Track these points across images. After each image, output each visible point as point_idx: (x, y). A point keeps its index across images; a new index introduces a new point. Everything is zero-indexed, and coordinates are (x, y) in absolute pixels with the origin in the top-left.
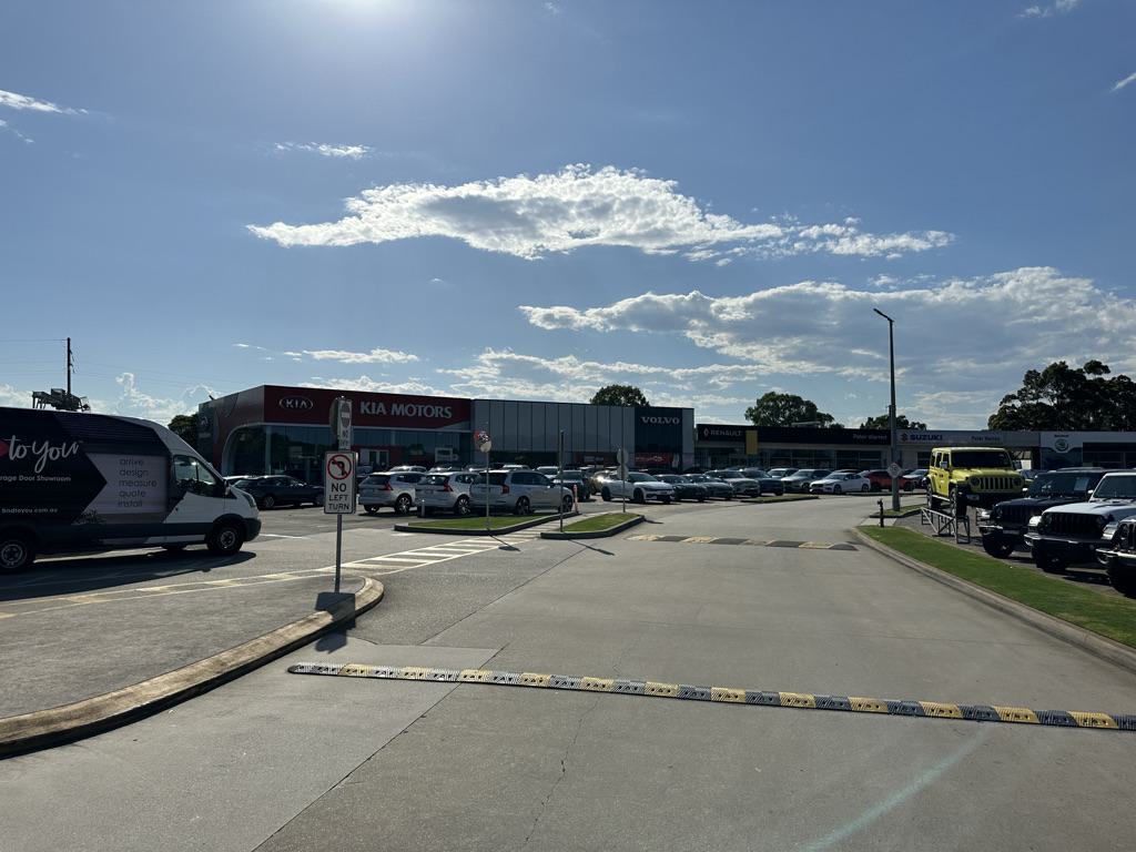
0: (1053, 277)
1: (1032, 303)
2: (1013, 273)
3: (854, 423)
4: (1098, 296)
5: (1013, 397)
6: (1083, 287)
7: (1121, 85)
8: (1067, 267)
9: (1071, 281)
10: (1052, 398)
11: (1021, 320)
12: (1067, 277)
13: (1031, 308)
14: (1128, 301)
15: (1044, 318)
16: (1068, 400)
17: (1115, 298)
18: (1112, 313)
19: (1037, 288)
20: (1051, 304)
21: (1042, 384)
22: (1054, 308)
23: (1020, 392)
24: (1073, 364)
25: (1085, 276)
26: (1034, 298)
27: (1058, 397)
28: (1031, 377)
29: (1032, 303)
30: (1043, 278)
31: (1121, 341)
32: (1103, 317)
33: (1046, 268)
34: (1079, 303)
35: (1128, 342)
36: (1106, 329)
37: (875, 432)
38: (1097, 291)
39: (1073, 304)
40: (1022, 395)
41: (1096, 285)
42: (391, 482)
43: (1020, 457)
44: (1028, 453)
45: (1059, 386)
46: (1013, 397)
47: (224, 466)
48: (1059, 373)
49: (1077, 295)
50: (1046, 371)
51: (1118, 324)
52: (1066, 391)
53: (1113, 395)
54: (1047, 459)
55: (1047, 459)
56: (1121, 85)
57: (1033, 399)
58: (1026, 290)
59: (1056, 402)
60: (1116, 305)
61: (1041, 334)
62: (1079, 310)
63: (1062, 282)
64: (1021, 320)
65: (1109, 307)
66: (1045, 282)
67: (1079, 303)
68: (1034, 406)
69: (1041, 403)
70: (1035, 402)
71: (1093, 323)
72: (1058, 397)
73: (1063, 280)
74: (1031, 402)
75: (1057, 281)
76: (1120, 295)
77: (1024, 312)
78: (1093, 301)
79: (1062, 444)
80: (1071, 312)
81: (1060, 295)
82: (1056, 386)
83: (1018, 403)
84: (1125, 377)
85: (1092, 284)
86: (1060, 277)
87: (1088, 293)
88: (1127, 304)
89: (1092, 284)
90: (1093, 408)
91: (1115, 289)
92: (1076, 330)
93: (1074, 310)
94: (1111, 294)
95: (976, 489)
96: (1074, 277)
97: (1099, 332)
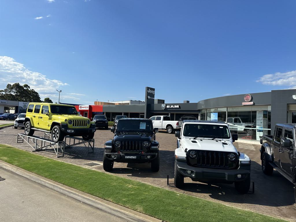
0: (14, 61)
1: (7, 67)
2: (2, 57)
3: (21, 82)
4: (24, 69)
5: (3, 91)
6: (21, 66)
7: (37, 18)
8: (17, 59)
9: (18, 63)
10: (15, 92)
11: (3, 71)
12: (17, 62)
13: (6, 68)
14: (31, 72)
15: (10, 72)
16: (19, 94)
17: (28, 70)
18: (27, 74)
19: (8, 63)
20: (12, 68)
21: (12, 88)
22: (13, 69)
23: (5, 90)
24: (22, 84)
25: (22, 63)
26: (7, 66)
27: (16, 93)
28: (9, 86)
29: (8, 67)
30: (11, 61)
31: (28, 81)
32: (25, 75)
33: (12, 58)
34: (19, 69)
35: (30, 82)
36: (25, 78)
37: (27, 92)
38: (24, 68)
39: (18, 70)
40: (6, 90)
41: (24, 66)
42: (269, 115)
43: (11, 109)
44: (14, 108)
45: (17, 90)
46: (3, 91)
47: (129, 117)
48: (17, 86)
49: (19, 67)
50: (14, 85)
51: (28, 77)
52: (18, 91)
53: (30, 94)
54: (20, 110)
55: (20, 110)
56: (37, 18)
57: (8, 92)
58: (5, 62)
59: (15, 94)
60: (28, 72)
61: (8, 76)
62: (19, 72)
63: (16, 63)
64: (3, 71)
65: (27, 72)
66: (11, 62)
67: (19, 69)
68: (9, 94)
69: (11, 94)
70: (9, 93)
71: (22, 76)
72: (16, 93)
73: (16, 62)
74: (8, 93)
75: (14, 62)
76: (29, 70)
77: (4, 68)
78: (23, 70)
79: (25, 106)
80: (17, 72)
81: (15, 66)
82: (16, 90)
83: (4, 93)
84: (33, 90)
85: (23, 65)
86: (15, 62)
87: (22, 68)
88: (31, 73)
89: (23, 65)
90: (25, 97)
91: (29, 68)
92: (18, 76)
93: (18, 71)
94: (28, 69)
95: (70, 126)
96: (19, 62)
97: (23, 78)
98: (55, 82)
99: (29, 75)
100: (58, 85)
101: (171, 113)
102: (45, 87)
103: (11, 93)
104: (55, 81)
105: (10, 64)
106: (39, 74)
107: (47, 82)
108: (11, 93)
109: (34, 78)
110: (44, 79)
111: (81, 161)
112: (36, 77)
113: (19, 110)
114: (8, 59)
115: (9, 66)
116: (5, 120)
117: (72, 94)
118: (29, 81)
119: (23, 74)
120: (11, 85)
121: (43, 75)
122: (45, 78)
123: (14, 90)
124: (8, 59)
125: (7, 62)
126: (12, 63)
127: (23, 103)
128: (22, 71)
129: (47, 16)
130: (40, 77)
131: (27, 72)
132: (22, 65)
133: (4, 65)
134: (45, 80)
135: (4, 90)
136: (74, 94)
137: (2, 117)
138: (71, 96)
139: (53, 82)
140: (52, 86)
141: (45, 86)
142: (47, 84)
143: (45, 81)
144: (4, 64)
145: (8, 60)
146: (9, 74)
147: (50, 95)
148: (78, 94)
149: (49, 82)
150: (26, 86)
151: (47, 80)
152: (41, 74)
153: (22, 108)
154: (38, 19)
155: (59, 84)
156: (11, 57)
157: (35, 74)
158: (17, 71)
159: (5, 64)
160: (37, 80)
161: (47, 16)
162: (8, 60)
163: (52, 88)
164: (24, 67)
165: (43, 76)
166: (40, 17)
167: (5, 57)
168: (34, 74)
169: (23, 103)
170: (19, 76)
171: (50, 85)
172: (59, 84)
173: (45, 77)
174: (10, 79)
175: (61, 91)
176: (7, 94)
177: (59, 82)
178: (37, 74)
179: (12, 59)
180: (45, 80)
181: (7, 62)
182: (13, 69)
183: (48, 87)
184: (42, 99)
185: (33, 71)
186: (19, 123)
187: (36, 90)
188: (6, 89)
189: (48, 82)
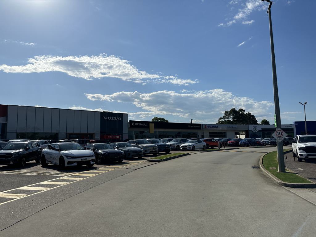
0: (224, 91)
5: (222, 118)
6: (230, 94)
7: (240, 45)
8: (226, 89)
9: (227, 92)
11: (216, 102)
12: (226, 91)
13: (218, 99)
15: (221, 101)
18: (236, 100)
19: (219, 94)
21: (229, 114)
22: (223, 99)
23: (223, 117)
24: (237, 110)
27: (234, 118)
29: (219, 98)
31: (238, 107)
32: (234, 102)
34: (229, 98)
38: (233, 95)
39: (228, 98)
43: (241, 134)
48: (233, 111)
49: (229, 96)
51: (237, 103)
56: (240, 45)
58: (217, 94)
61: (220, 106)
62: (229, 100)
63: (225, 92)
65: (235, 99)
67: (229, 98)
72: (234, 118)
73: (225, 92)
76: (237, 96)
78: (232, 97)
80: (227, 100)
81: (225, 96)
82: (233, 115)
83: (223, 120)
84: (250, 113)
87: (231, 96)
88: (239, 98)
92: (228, 105)
93: (228, 99)
96: (228, 91)
98: (264, 103)
99: (238, 101)
100: (267, 106)
101: (296, 135)
102: (254, 110)
103: (229, 119)
104: (264, 102)
105: (221, 95)
106: (247, 98)
107: (256, 105)
108: (229, 119)
109: (242, 103)
110: (252, 103)
111: (299, 190)
112: (244, 102)
113: (249, 135)
114: (219, 91)
115: (220, 96)
116: (248, 146)
117: (285, 113)
118: (238, 107)
119: (232, 101)
120: (228, 112)
121: (251, 99)
122: (253, 101)
123: (231, 116)
124: (219, 91)
125: (218, 93)
126: (222, 93)
127: (253, 126)
128: (231, 99)
129: (249, 39)
130: (248, 101)
131: (235, 99)
132: (231, 93)
133: (216, 97)
134: (254, 103)
135: (223, 117)
136: (287, 113)
137: (243, 143)
138: (284, 116)
139: (262, 104)
140: (261, 109)
141: (254, 109)
142: (256, 107)
143: (254, 104)
144: (216, 95)
145: (219, 92)
146: (221, 104)
147: (260, 118)
148: (292, 112)
149: (258, 104)
150: (241, 110)
151: (255, 103)
152: (248, 98)
153: (253, 131)
154: (241, 45)
155: (269, 105)
156: (221, 89)
157: (243, 100)
158: (227, 99)
159: (217, 96)
160: (245, 104)
161: (249, 39)
162: (219, 92)
163: (261, 110)
164: (233, 94)
165: (251, 100)
166: (243, 42)
167: (216, 89)
168: (242, 99)
169: (253, 126)
170: (229, 103)
171: (259, 108)
172: (268, 104)
173: (253, 100)
174: (222, 108)
175: (306, 103)
176: (225, 121)
177: (268, 102)
178: (245, 99)
179: (222, 90)
180: (254, 103)
181: (218, 93)
182: (223, 99)
183: (258, 110)
184: (259, 122)
185: (241, 97)
186: (307, 152)
187: (252, 113)
188: (225, 116)
189: (256, 105)
